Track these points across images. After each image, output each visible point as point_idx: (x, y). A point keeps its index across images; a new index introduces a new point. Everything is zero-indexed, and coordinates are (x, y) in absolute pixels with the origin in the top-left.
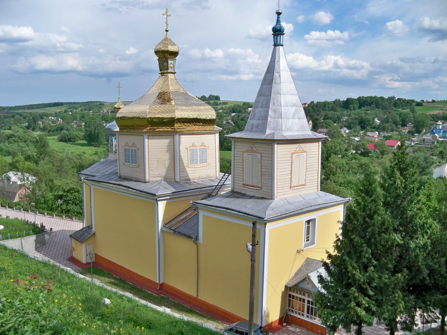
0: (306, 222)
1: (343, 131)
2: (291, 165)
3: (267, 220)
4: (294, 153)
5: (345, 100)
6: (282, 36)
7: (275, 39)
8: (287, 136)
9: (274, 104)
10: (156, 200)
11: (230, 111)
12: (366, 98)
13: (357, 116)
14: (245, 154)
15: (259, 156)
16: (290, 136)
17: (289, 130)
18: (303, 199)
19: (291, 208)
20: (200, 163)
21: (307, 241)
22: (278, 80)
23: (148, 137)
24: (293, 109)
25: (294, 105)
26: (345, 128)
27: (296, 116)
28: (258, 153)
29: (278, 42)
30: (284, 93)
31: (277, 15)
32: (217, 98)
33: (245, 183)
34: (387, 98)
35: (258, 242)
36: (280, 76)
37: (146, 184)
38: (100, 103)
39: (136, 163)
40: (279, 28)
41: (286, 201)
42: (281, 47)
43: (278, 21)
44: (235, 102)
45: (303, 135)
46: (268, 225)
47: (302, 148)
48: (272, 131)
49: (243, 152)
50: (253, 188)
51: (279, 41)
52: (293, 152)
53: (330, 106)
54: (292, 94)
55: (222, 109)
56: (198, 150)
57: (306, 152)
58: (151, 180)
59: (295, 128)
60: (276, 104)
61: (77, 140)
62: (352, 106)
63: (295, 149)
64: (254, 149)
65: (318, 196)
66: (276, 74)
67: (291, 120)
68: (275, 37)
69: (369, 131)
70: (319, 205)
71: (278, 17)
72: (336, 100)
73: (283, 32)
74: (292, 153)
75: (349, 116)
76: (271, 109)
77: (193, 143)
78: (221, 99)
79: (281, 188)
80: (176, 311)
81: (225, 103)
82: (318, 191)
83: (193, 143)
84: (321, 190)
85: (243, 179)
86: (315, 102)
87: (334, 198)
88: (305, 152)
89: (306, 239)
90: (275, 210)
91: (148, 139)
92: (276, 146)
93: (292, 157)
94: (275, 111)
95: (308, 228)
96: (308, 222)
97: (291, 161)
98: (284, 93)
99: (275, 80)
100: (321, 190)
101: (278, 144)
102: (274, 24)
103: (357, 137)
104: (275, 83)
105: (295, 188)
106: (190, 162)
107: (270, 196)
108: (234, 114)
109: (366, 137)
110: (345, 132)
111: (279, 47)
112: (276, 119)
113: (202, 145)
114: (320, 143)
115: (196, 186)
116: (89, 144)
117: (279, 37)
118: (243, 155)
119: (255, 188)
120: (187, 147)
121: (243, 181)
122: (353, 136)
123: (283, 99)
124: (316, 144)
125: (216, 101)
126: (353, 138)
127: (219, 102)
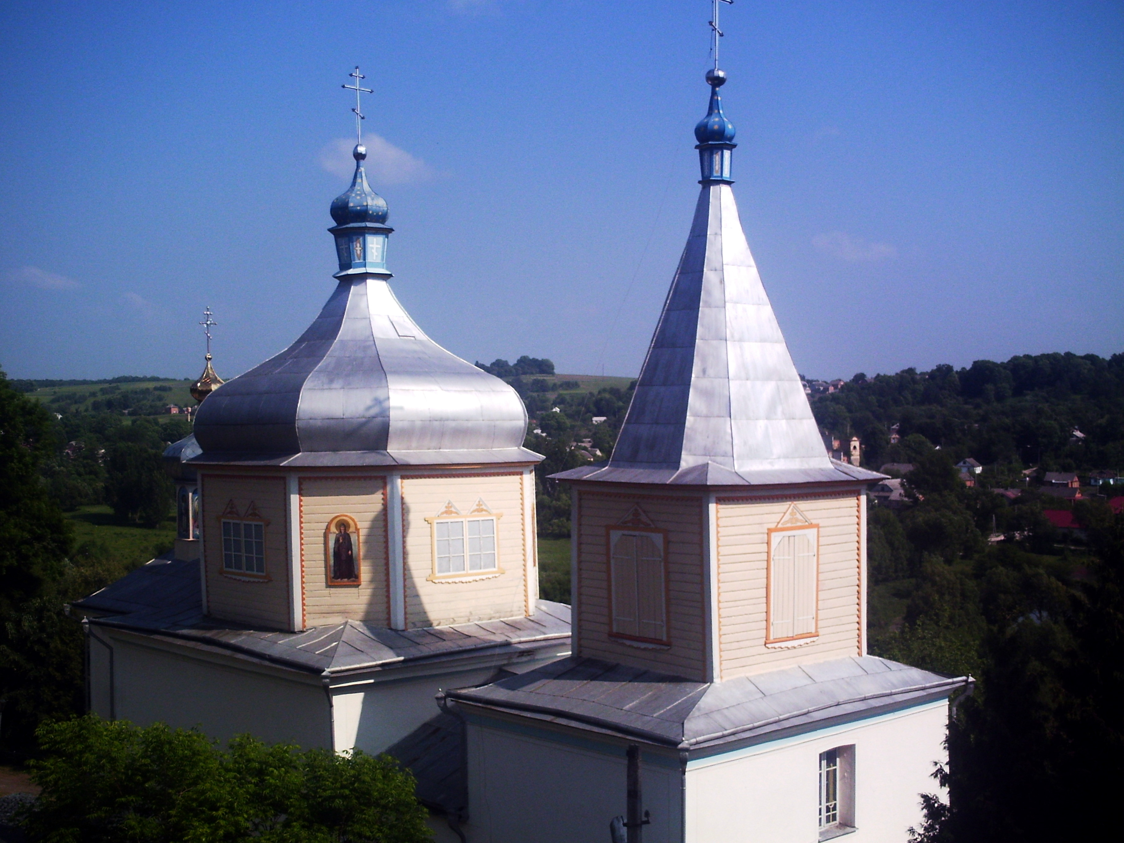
0: (821, 756)
1: (964, 470)
2: (768, 569)
3: (686, 750)
4: (777, 530)
5: (969, 366)
6: (727, 153)
7: (706, 164)
8: (750, 474)
9: (704, 371)
10: (326, 687)
11: (588, 411)
12: (1036, 360)
13: (1007, 421)
14: (615, 536)
15: (658, 539)
16: (759, 474)
17: (754, 454)
18: (808, 681)
19: (769, 711)
20: (472, 567)
21: (828, 821)
22: (716, 293)
23: (300, 484)
24: (768, 389)
25: (769, 375)
26: (971, 460)
27: (779, 409)
28: (656, 530)
29: (716, 174)
30: (737, 336)
31: (710, 88)
32: (544, 367)
33: (615, 630)
34: (1108, 358)
35: (647, 814)
36: (722, 281)
37: (293, 637)
38: (159, 384)
39: (260, 569)
40: (716, 127)
41: (752, 687)
42: (725, 190)
43: (713, 106)
44: (603, 379)
45: (805, 472)
46: (690, 766)
47: (801, 512)
48: (701, 460)
49: (609, 528)
50: (643, 645)
51: (717, 167)
52: (773, 526)
53: (921, 387)
54: (763, 340)
55: (560, 401)
56: (466, 525)
57: (817, 526)
58: (309, 623)
59: (777, 450)
60: (710, 372)
61: (81, 504)
62: (990, 387)
63: (776, 518)
64: (643, 518)
65: (860, 672)
66: (709, 275)
67: (762, 423)
68: (706, 157)
69: (1051, 471)
70: (865, 699)
71: (714, 93)
72: (940, 368)
73: (731, 138)
74: (770, 531)
75: (984, 419)
76: (696, 388)
77: (449, 505)
78: (557, 371)
79: (735, 645)
80: (319, 423)
81: (570, 384)
82: (860, 654)
83: (449, 505)
84: (868, 653)
85: (610, 616)
86: (870, 375)
87: (916, 677)
88: (811, 526)
89: (824, 814)
90: (718, 717)
91: (301, 494)
92: (713, 507)
93: (768, 543)
94: (708, 394)
95: (831, 777)
96: (830, 757)
97: (764, 556)
98: (737, 336)
99: (709, 293)
100: (868, 653)
101: (720, 501)
102: (699, 115)
103: (1013, 487)
104: (708, 305)
105: (783, 645)
106: (440, 565)
107: (696, 668)
108: (603, 419)
109: (1042, 489)
110: (972, 474)
111: (717, 187)
112: (713, 421)
113: (479, 510)
114: (863, 498)
115: (460, 643)
116: (118, 520)
117: (717, 158)
118: (608, 536)
119: (651, 646)
120: (428, 515)
121: (610, 624)
122: (998, 485)
123: (734, 356)
124: (850, 502)
125: (540, 377)
126: (997, 491)
127: (548, 378)
